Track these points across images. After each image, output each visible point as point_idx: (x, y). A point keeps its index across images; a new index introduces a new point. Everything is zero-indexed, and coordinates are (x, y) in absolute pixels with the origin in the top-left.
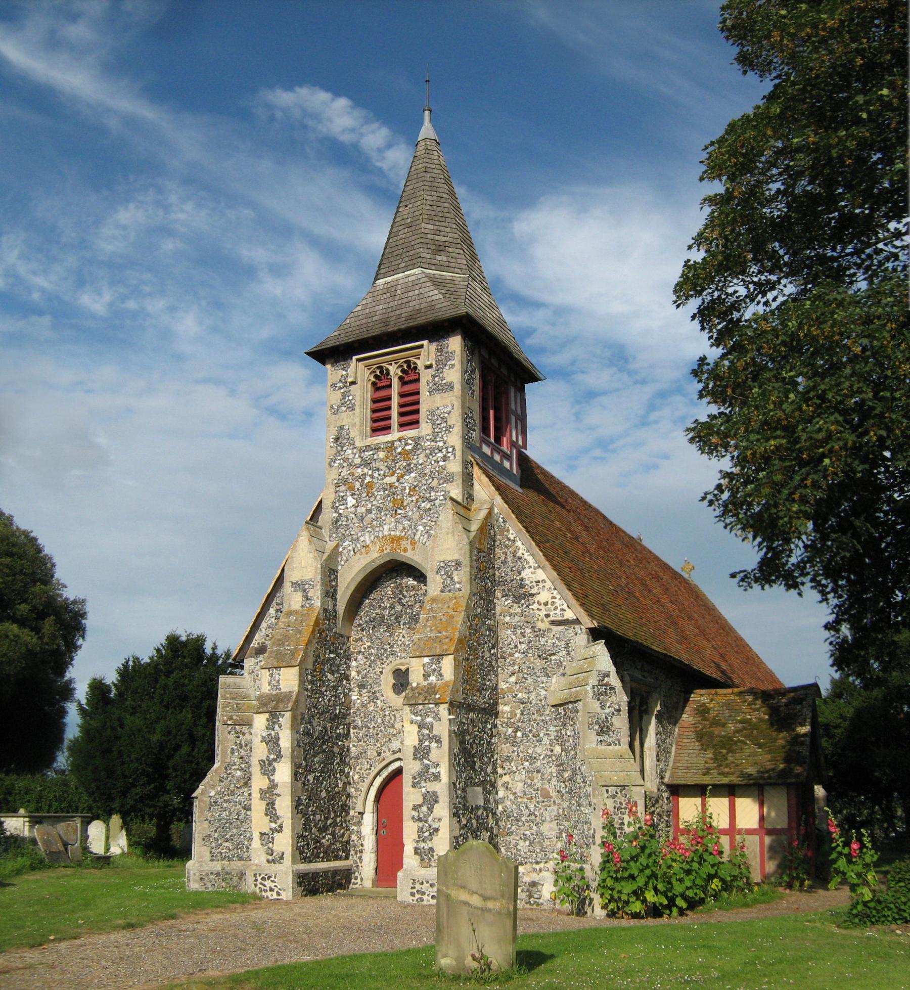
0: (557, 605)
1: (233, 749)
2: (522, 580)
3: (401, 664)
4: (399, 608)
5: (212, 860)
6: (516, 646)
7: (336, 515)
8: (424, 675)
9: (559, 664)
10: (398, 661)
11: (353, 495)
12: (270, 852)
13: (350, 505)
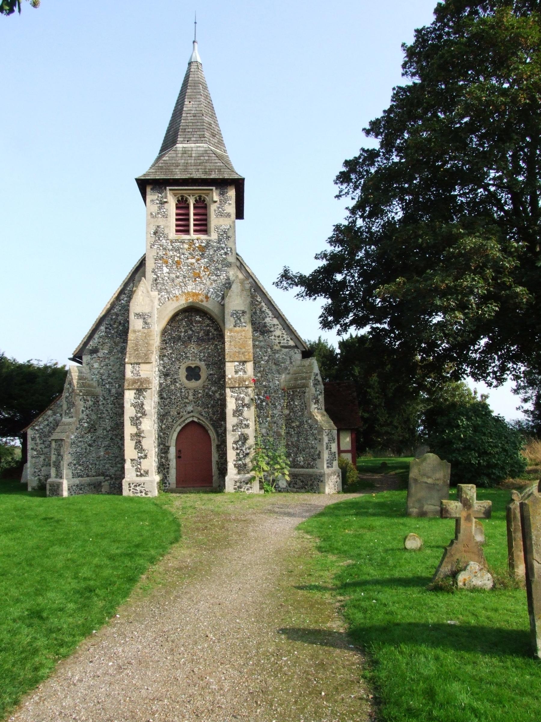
0: (285, 337)
1: (83, 410)
2: (265, 323)
3: (192, 364)
4: (190, 332)
5: (73, 478)
6: (262, 358)
7: (155, 276)
8: (235, 372)
9: (286, 368)
10: (190, 362)
11: (167, 266)
12: (138, 470)
13: (164, 272)
